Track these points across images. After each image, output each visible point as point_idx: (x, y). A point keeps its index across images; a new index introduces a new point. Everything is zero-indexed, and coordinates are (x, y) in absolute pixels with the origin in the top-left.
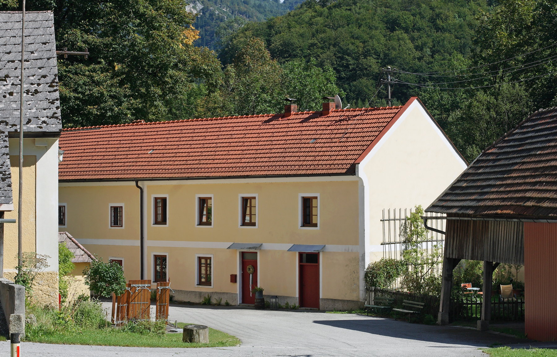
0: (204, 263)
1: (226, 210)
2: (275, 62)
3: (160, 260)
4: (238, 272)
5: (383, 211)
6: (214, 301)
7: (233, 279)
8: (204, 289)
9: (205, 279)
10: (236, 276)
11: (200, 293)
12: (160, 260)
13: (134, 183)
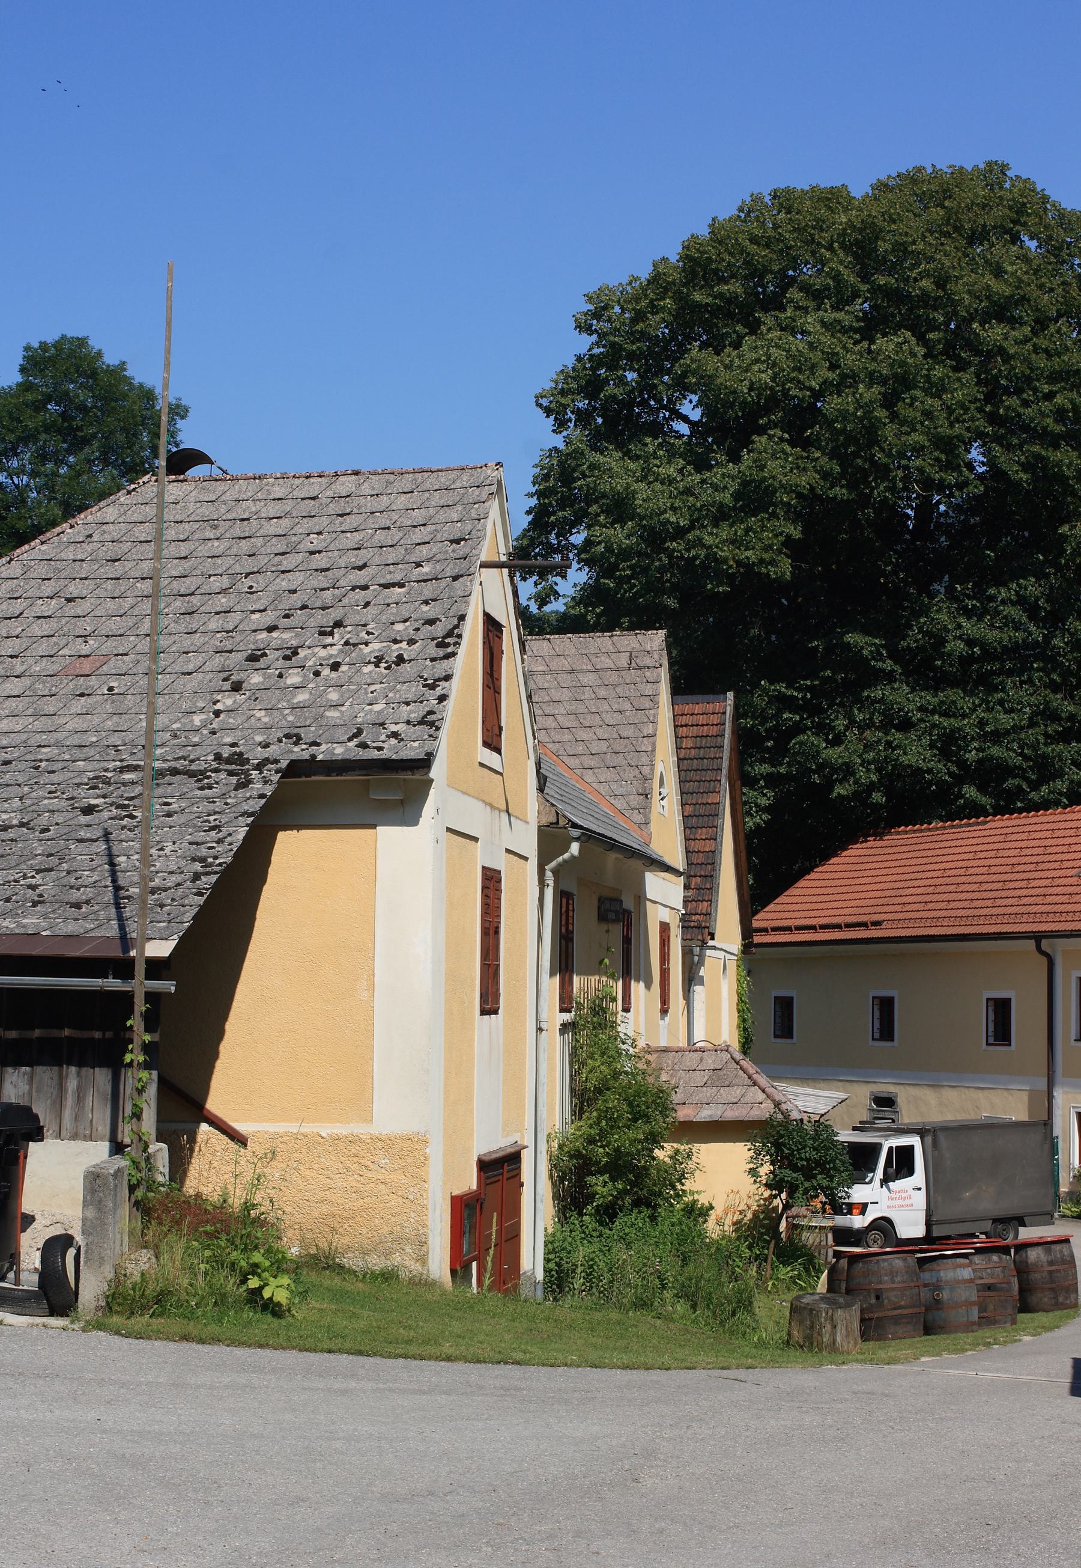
13: (1032, 943)
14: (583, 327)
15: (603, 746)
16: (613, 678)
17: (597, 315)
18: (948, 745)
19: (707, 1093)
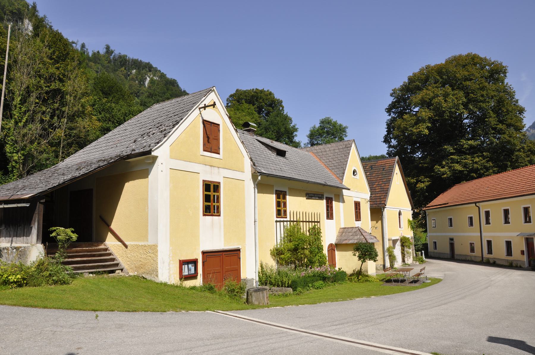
0: (509, 244)
1: (516, 216)
2: (370, 241)
3: (489, 243)
4: (524, 248)
5: (488, 222)
6: (514, 265)
7: (522, 252)
8: (509, 258)
9: (509, 252)
10: (523, 251)
11: (508, 260)
12: (489, 243)
13: (474, 205)
14: (391, 95)
15: (337, 164)
16: (342, 150)
17: (394, 93)
18: (465, 166)
19: (351, 237)
